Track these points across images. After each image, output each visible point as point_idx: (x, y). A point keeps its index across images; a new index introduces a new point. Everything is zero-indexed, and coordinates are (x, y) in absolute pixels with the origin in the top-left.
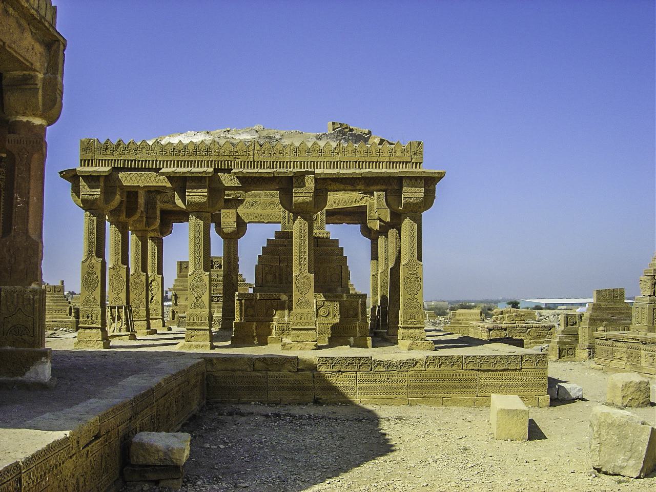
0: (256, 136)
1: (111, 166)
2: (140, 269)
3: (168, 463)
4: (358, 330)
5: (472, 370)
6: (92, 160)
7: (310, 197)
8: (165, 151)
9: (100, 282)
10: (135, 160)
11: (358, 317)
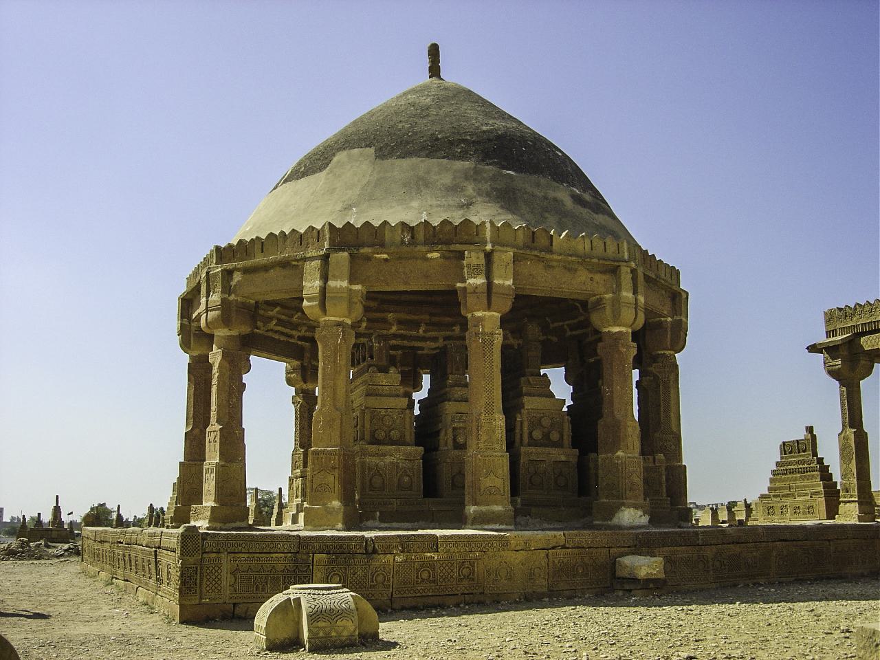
3: (632, 576)
6: (836, 330)
10: (871, 322)
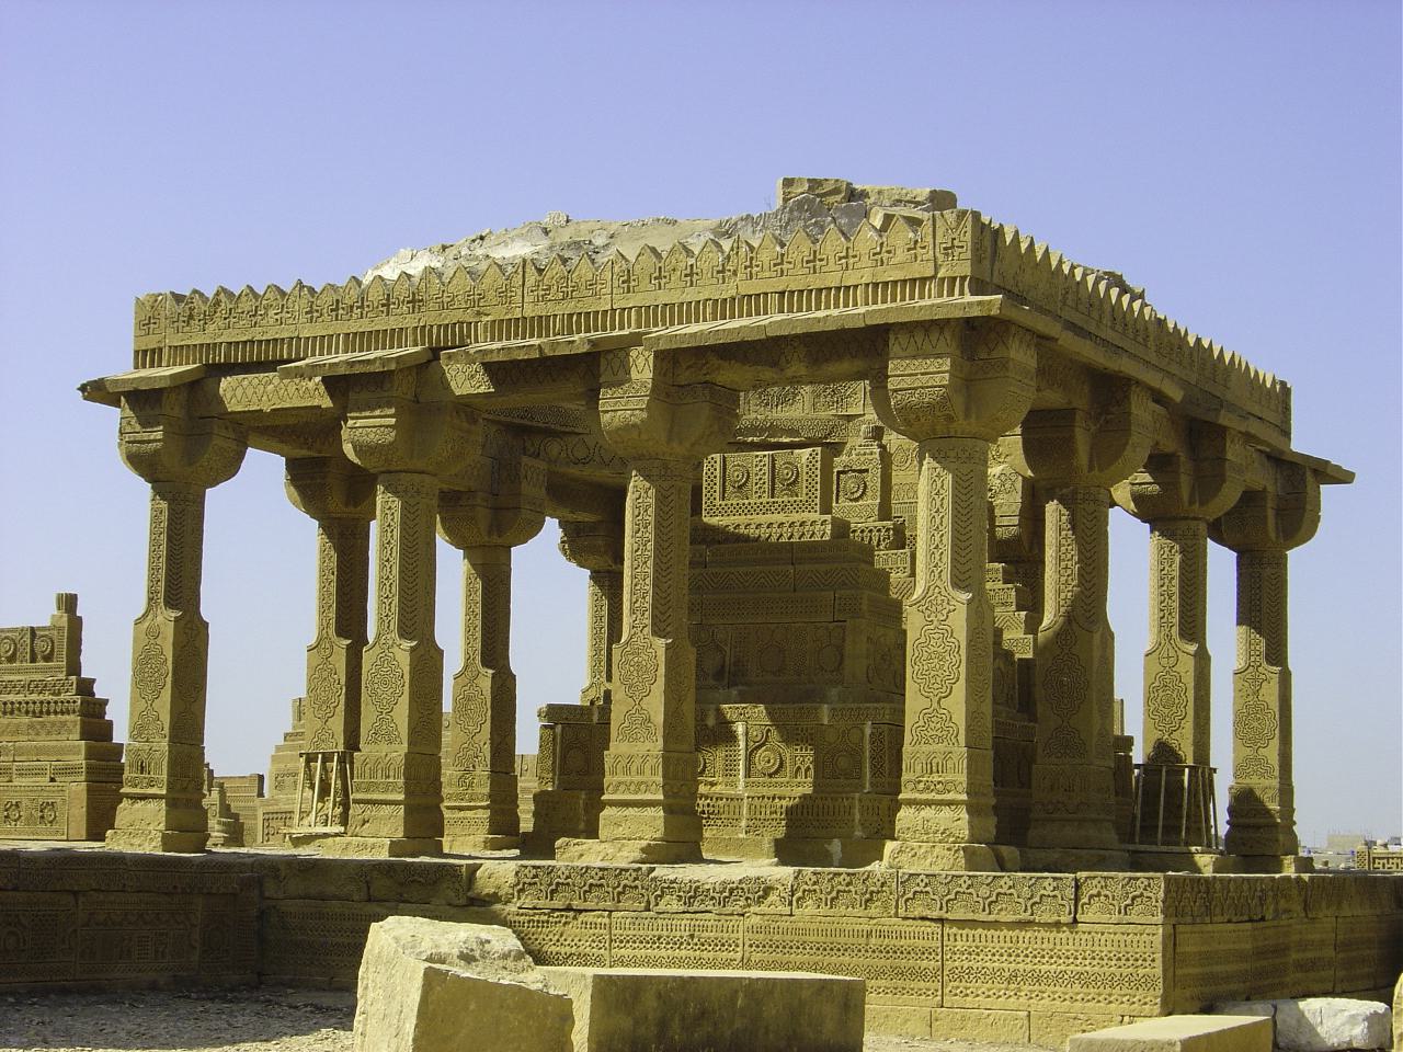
0: (544, 243)
1: (201, 360)
2: (478, 658)
4: (857, 816)
5: (923, 919)
7: (641, 410)
8: (317, 311)
9: (170, 675)
11: (860, 777)
